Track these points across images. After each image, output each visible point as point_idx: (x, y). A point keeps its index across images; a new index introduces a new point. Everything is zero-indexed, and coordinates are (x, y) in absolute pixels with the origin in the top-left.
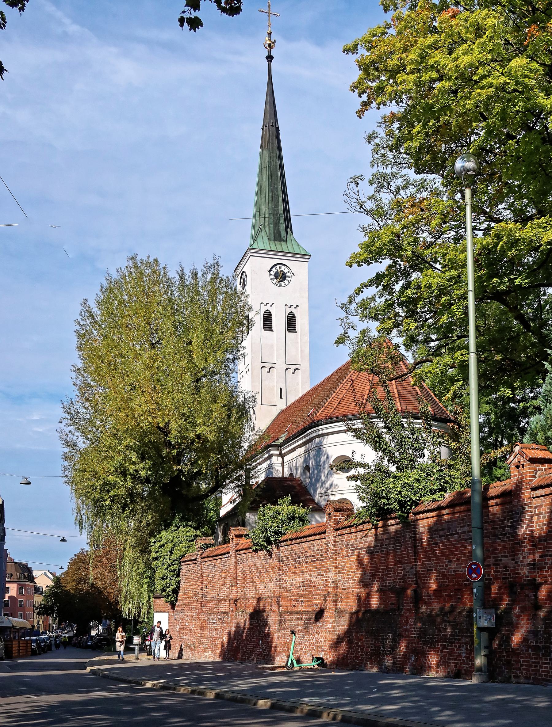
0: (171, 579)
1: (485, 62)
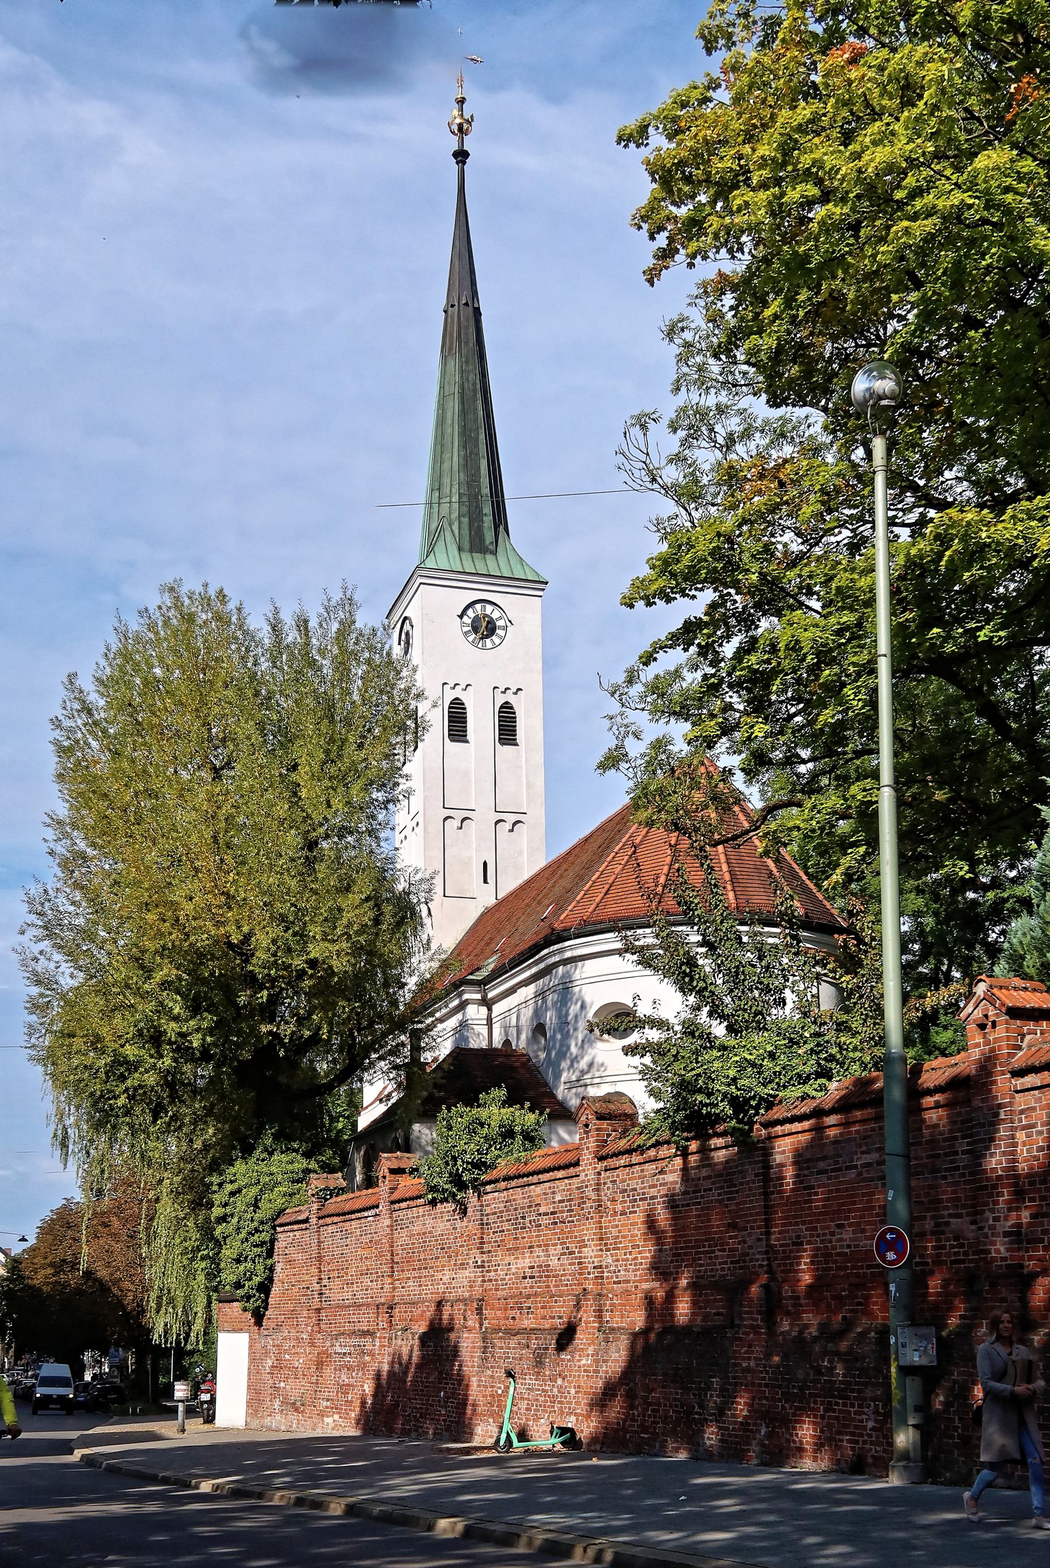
0: (254, 1262)
1: (921, 160)
